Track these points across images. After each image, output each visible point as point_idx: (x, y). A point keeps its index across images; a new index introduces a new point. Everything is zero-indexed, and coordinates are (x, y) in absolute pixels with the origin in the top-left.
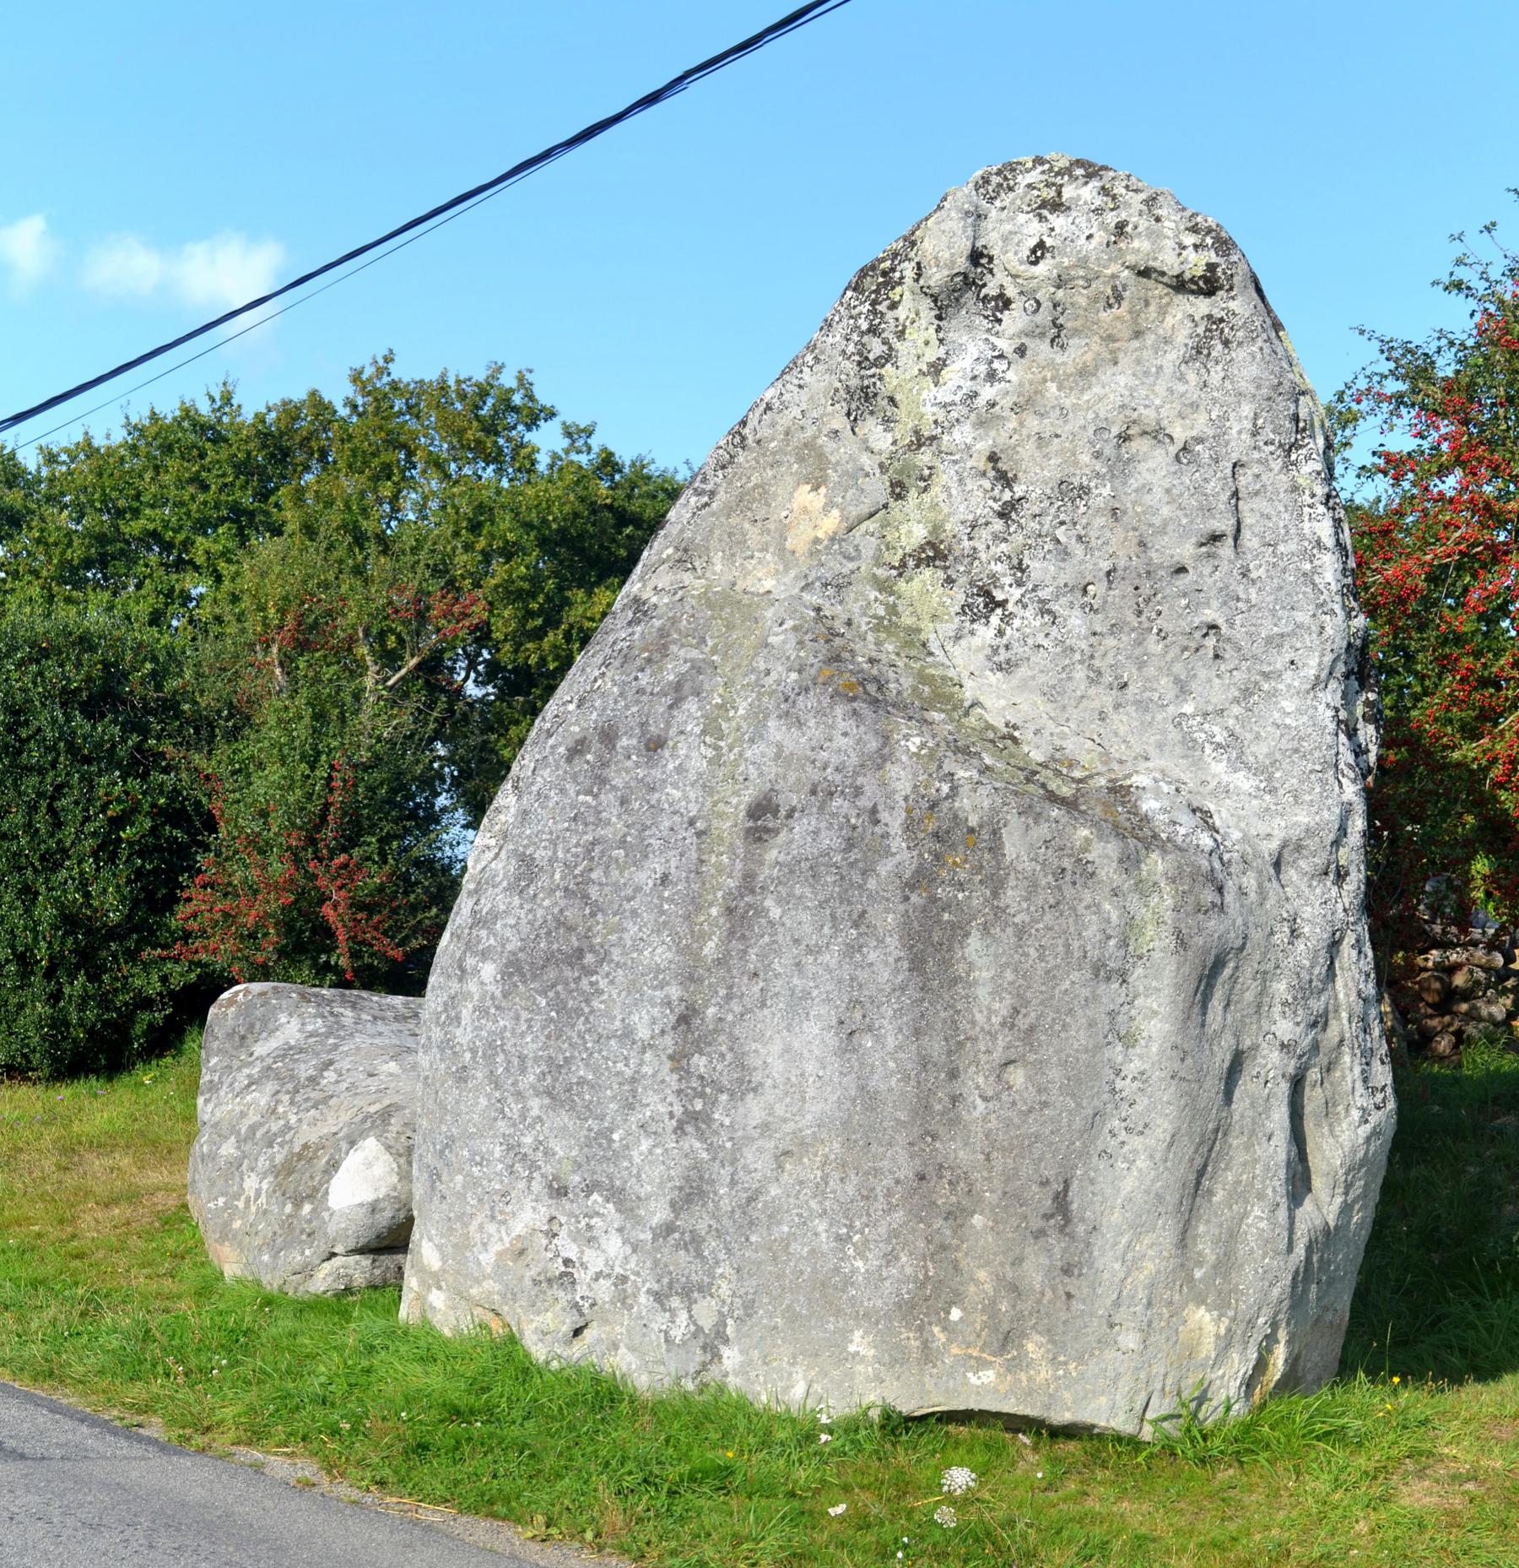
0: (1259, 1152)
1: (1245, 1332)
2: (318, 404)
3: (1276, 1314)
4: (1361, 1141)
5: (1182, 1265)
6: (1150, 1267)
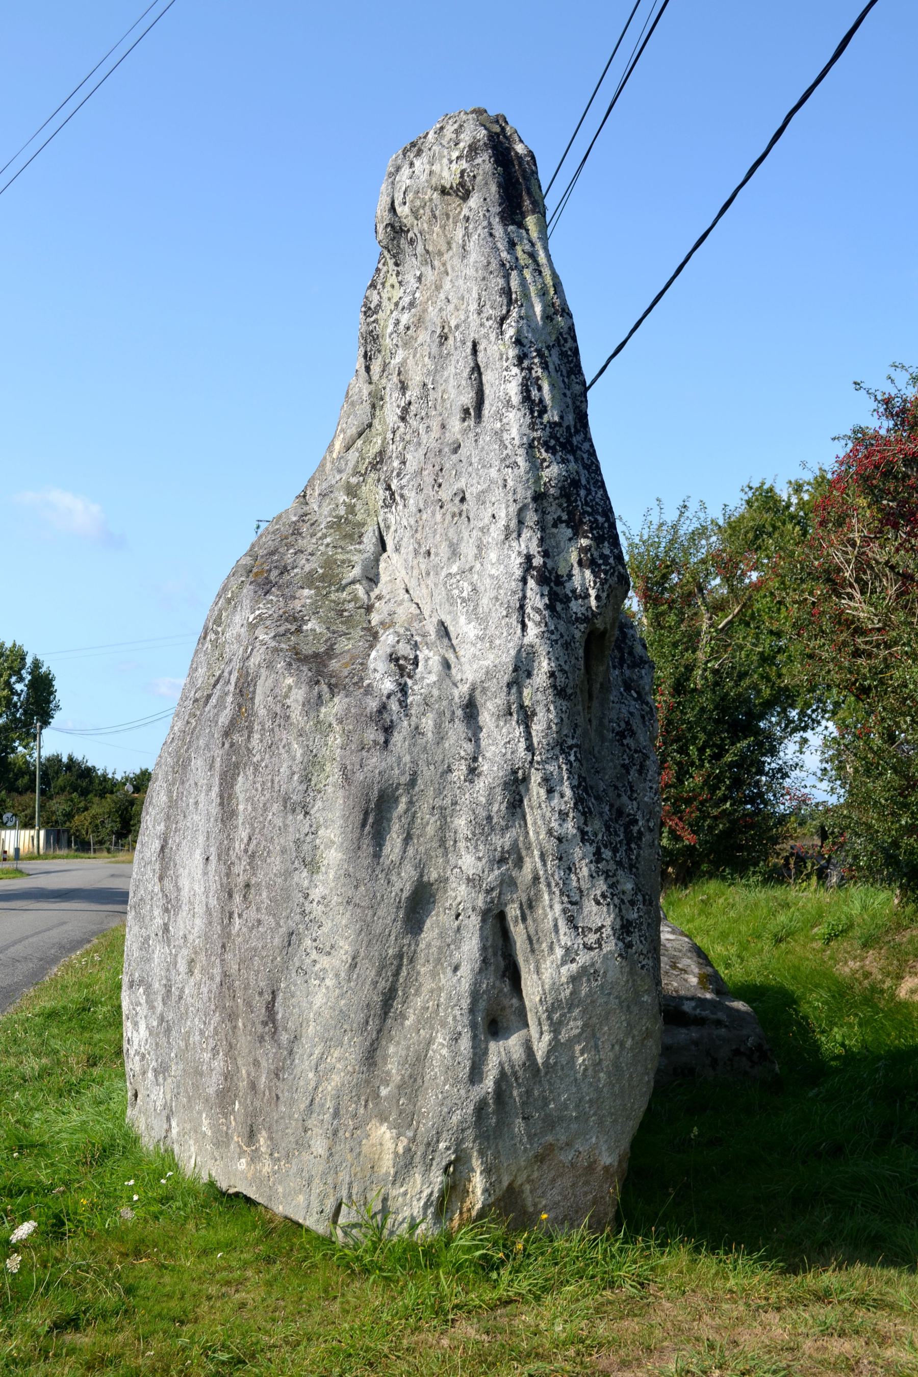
0: (443, 981)
1: (424, 1156)
2: (861, 437)
3: (459, 1142)
4: (564, 980)
5: (367, 1082)
6: (336, 1079)
